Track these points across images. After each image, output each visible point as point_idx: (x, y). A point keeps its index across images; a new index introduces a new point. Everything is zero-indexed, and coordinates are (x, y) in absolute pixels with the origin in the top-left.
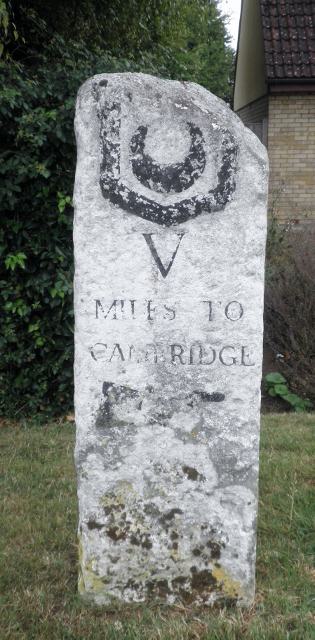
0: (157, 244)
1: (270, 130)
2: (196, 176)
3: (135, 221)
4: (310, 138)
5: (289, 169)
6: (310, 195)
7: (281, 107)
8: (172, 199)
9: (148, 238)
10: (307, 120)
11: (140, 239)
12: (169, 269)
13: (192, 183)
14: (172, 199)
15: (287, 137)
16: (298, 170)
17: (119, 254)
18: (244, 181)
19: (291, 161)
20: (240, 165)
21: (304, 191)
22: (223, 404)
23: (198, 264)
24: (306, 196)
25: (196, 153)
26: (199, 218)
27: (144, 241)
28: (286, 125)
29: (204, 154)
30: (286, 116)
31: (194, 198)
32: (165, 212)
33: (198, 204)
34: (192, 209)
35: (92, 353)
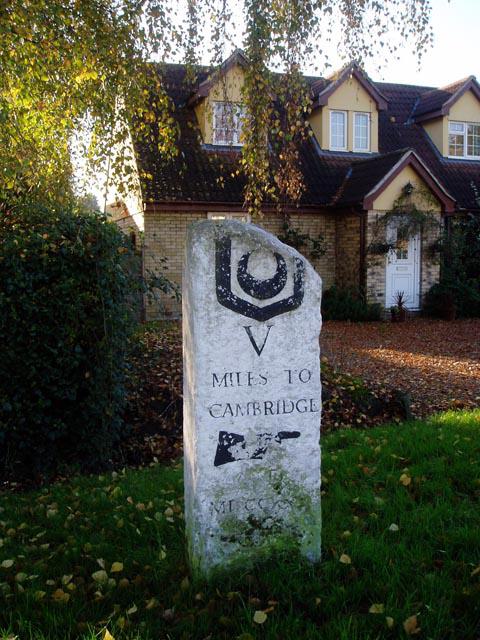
25: (282, 270)
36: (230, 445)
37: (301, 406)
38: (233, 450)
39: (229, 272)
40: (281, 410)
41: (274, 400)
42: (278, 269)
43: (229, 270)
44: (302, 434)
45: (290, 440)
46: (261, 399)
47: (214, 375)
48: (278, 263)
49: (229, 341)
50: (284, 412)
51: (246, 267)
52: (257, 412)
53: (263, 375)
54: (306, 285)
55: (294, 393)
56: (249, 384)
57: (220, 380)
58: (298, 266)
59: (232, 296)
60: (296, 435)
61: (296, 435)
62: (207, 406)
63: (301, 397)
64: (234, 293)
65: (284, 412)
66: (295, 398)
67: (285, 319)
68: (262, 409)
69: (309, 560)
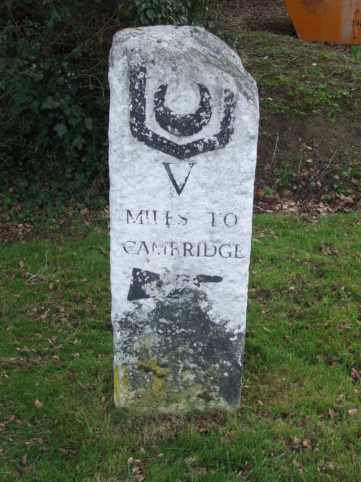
2: (204, 124)
3: (156, 154)
11: (161, 166)
25: (204, 106)
33: (205, 144)
34: (200, 147)
36: (144, 283)
37: (225, 251)
38: (147, 288)
39: (144, 104)
40: (202, 252)
41: (195, 242)
42: (202, 103)
43: (144, 102)
44: (224, 279)
45: (211, 284)
46: (180, 240)
47: (129, 212)
48: (202, 97)
49: (145, 178)
50: (205, 255)
51: (163, 100)
52: (175, 252)
53: (182, 215)
54: (237, 121)
55: (217, 237)
56: (167, 223)
57: (135, 217)
58: (226, 100)
59: (147, 131)
60: (217, 279)
61: (217, 279)
62: (121, 241)
63: (227, 241)
64: (149, 127)
65: (205, 255)
66: (218, 241)
67: (210, 158)
68: (182, 251)
69: (308, 442)
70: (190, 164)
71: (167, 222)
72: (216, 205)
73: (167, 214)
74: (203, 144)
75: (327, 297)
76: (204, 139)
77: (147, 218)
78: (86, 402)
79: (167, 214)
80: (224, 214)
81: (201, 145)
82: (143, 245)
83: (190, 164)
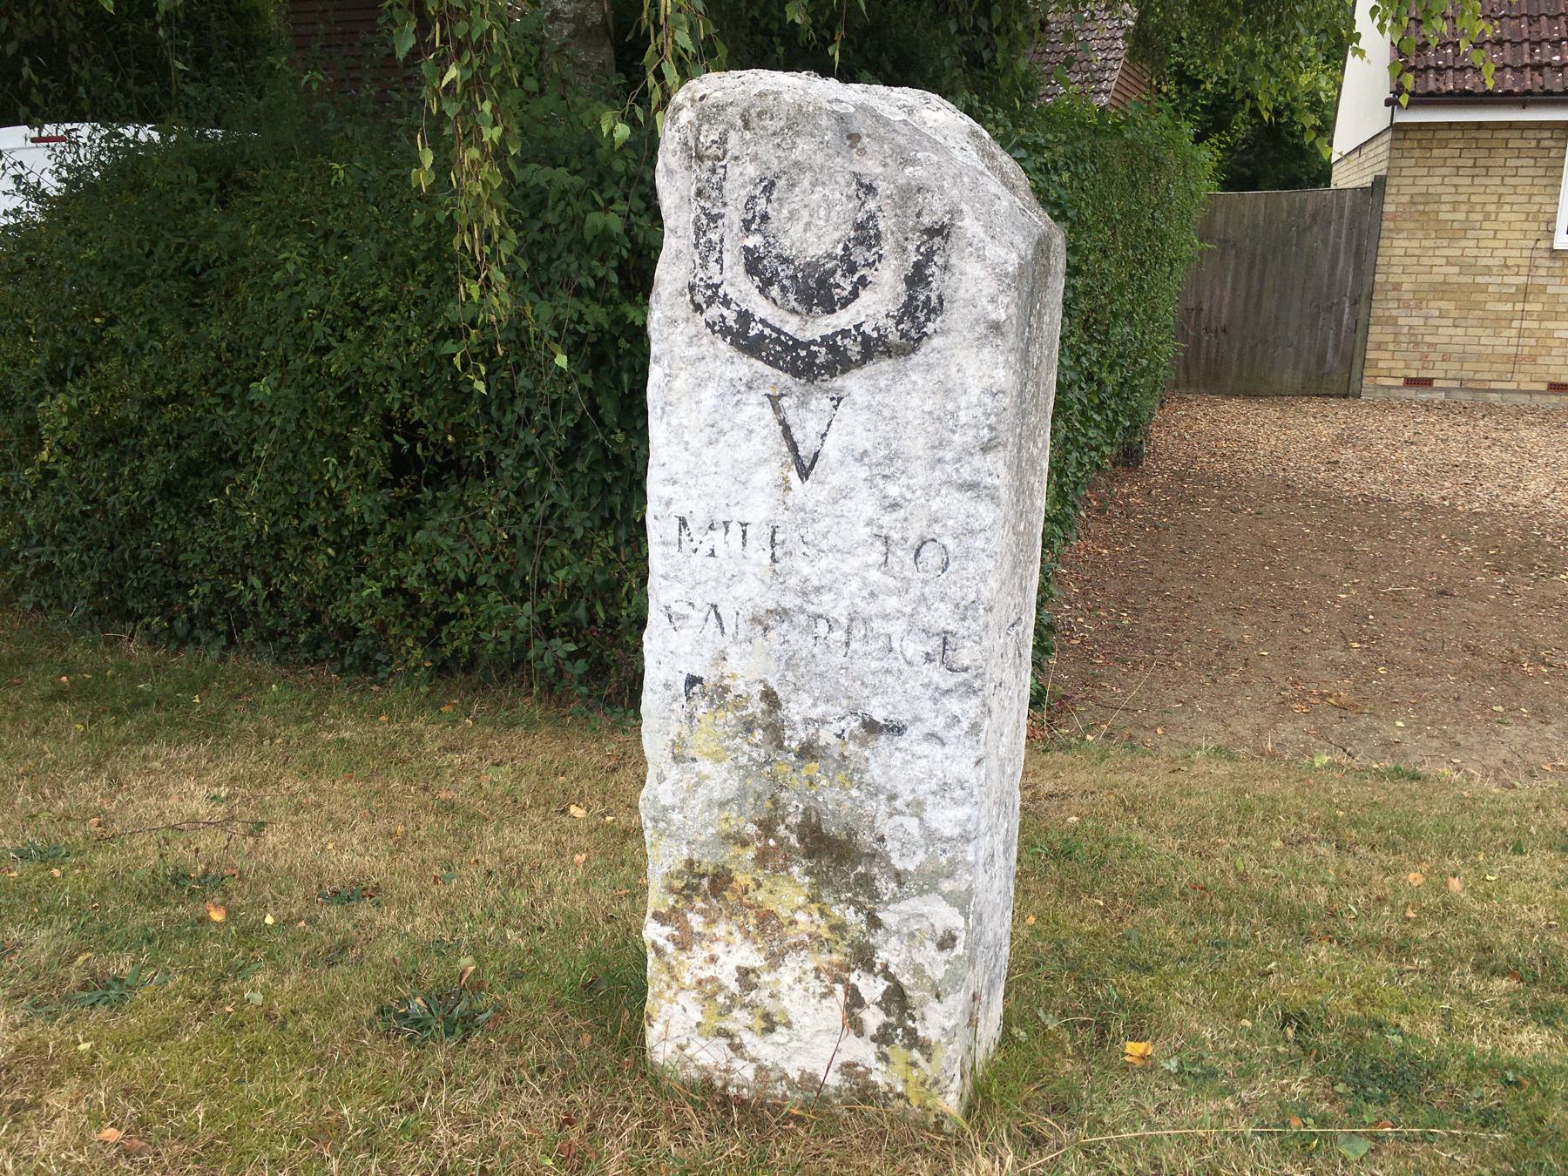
0: (791, 418)
1: (1387, 199)
2: (863, 282)
3: (747, 367)
4: (1473, 216)
5: (1421, 278)
6: (1460, 331)
7: (1417, 153)
8: (821, 326)
9: (774, 401)
10: (1468, 181)
11: (762, 404)
12: (812, 466)
13: (854, 295)
14: (821, 326)
15: (1423, 213)
16: (1441, 279)
17: (722, 433)
18: (961, 293)
19: (1424, 261)
20: (953, 261)
21: (1450, 322)
22: (902, 742)
23: (866, 460)
24: (1452, 331)
25: (866, 234)
26: (869, 368)
27: (768, 412)
28: (1424, 190)
29: (878, 236)
30: (1424, 171)
31: (857, 327)
32: (803, 353)
33: (866, 339)
34: (854, 350)
35: (670, 617)
70: (832, 399)
71: (773, 554)
72: (895, 515)
73: (774, 532)
74: (859, 339)
75: (1310, 208)
76: (861, 325)
77: (726, 543)
78: (1356, 1092)
79: (774, 532)
80: (914, 540)
81: (855, 340)
82: (712, 612)
83: (832, 399)
